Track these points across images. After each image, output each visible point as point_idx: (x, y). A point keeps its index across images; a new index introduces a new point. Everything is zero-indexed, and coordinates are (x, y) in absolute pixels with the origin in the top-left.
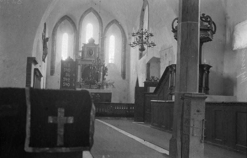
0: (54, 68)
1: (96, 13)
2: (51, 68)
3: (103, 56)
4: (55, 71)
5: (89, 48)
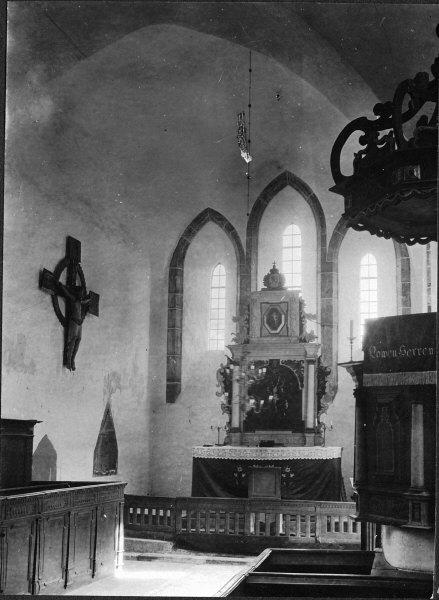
0: (179, 380)
1: (218, 218)
2: (168, 380)
3: (331, 326)
4: (183, 386)
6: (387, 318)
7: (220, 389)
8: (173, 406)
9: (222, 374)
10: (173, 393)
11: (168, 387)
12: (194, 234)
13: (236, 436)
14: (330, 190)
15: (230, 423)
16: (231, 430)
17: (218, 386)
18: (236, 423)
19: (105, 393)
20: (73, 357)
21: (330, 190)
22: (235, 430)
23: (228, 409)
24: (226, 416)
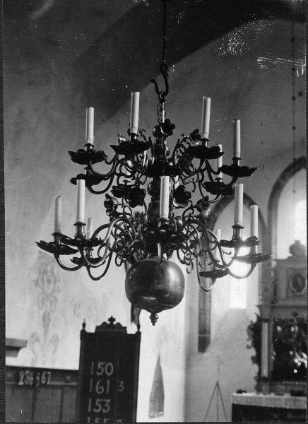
0: (209, 333)
2: (200, 333)
5: (291, 272)
6: (126, 290)
7: (250, 343)
8: (206, 355)
9: (252, 329)
10: (203, 344)
11: (200, 338)
12: (222, 210)
13: (265, 387)
14: (154, 325)
15: (260, 372)
16: (260, 379)
17: (248, 340)
18: (265, 373)
19: (157, 345)
20: (139, 315)
21: (154, 325)
22: (265, 379)
23: (257, 360)
24: (256, 368)
